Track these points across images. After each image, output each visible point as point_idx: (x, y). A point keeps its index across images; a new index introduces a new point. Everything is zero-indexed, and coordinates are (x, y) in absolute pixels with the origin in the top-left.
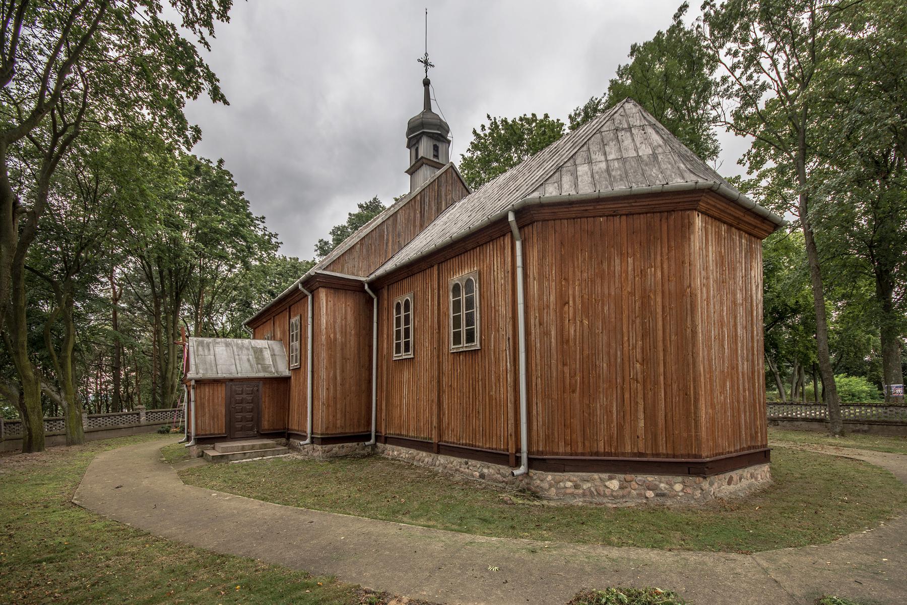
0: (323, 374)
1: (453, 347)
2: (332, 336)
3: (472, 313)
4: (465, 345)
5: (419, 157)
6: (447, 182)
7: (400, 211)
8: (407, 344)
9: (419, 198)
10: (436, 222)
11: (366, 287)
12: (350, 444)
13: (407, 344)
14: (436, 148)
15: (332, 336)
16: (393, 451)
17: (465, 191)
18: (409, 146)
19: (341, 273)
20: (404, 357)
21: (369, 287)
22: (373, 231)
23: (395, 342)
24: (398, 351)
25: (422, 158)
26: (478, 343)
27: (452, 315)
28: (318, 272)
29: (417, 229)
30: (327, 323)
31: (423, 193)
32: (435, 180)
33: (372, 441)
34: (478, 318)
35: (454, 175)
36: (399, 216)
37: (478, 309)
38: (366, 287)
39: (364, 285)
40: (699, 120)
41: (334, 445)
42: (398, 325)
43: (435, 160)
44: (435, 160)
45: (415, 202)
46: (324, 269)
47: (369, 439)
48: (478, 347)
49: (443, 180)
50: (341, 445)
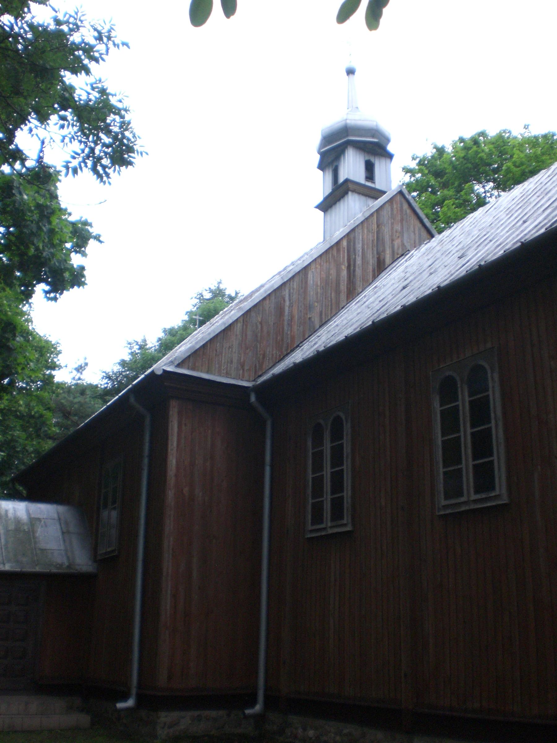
0: (464, 479)
1: (443, 502)
2: (186, 490)
3: (488, 433)
4: (474, 497)
5: (341, 179)
6: (393, 217)
7: (313, 266)
8: (338, 505)
9: (345, 243)
10: (377, 283)
11: (253, 398)
12: (213, 713)
13: (338, 505)
14: (370, 168)
15: (186, 490)
16: (305, 729)
17: (424, 233)
18: (322, 166)
19: (208, 372)
20: (330, 531)
21: (257, 398)
22: (264, 299)
23: (310, 501)
24: (318, 517)
25: (347, 181)
26: (504, 491)
27: (439, 440)
28: (169, 369)
29: (343, 296)
30: (178, 468)
31: (352, 236)
32: (372, 215)
33: (258, 708)
34: (350, 484)
35: (405, 206)
36: (310, 276)
37: (501, 424)
38: (253, 398)
39: (249, 396)
40: (130, 369)
41: (183, 714)
42: (318, 466)
43: (369, 184)
44: (369, 184)
45: (338, 250)
46: (178, 366)
47: (253, 703)
48: (505, 500)
49: (386, 213)
50: (196, 713)
